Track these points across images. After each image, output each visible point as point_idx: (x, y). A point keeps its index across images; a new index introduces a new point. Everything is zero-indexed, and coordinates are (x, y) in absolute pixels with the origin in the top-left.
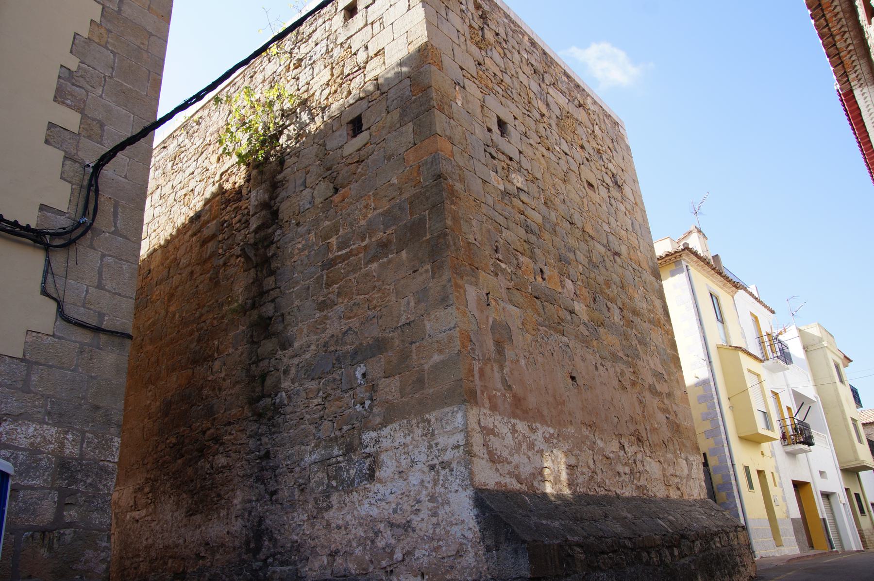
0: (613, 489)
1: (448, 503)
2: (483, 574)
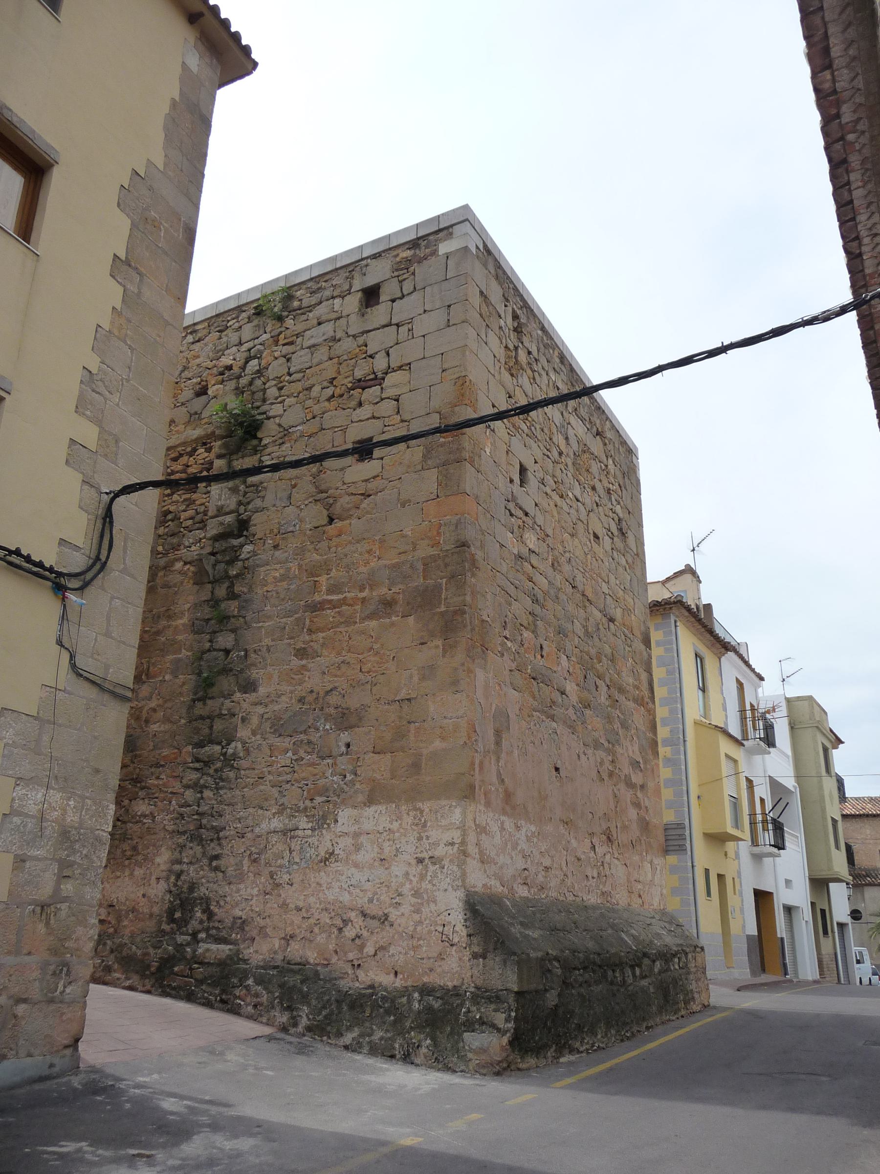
0: (580, 894)
1: (435, 902)
2: (465, 981)
